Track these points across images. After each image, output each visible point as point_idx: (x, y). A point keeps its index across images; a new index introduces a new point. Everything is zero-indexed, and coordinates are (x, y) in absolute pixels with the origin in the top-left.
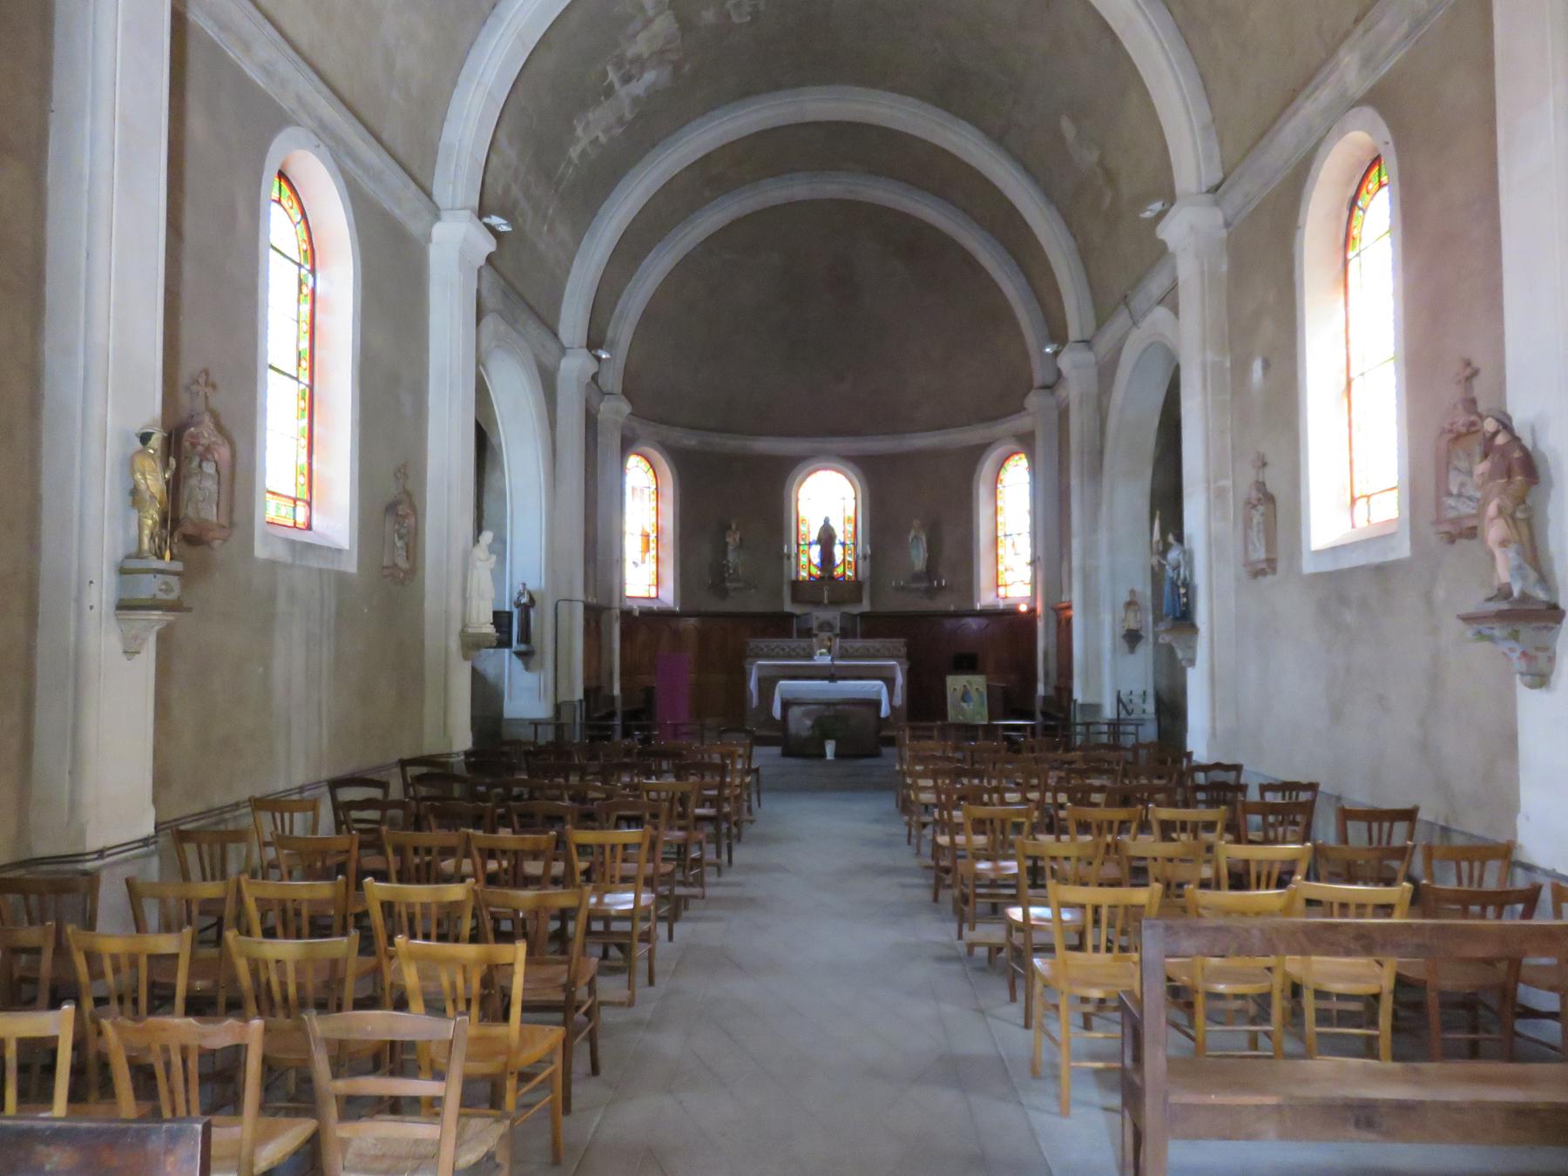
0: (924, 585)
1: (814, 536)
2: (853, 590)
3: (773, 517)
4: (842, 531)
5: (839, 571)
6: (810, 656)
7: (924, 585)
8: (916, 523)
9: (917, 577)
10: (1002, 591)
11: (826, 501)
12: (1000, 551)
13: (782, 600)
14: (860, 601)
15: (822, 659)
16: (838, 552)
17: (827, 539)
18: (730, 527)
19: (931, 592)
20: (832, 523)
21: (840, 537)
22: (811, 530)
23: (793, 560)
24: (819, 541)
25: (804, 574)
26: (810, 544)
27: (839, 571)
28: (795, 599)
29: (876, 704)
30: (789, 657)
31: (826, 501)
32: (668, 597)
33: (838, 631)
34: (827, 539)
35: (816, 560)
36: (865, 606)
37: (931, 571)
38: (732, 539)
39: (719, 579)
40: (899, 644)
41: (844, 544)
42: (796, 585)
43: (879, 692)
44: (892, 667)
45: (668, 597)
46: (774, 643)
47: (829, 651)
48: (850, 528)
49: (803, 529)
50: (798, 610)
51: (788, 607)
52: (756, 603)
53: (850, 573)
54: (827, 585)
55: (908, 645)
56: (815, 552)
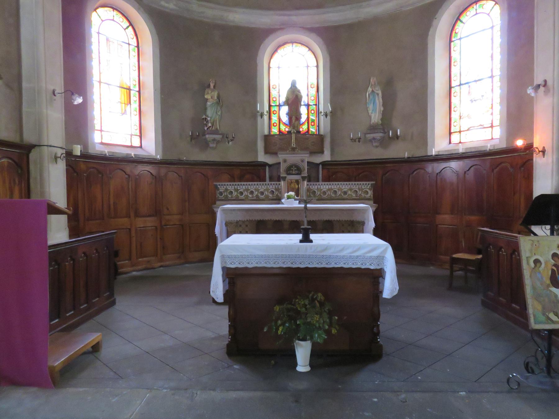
0: (378, 135)
1: (283, 99)
2: (316, 143)
3: (248, 81)
4: (307, 94)
5: (304, 128)
6: (278, 200)
7: (378, 135)
8: (373, 80)
9: (373, 128)
10: (455, 138)
11: (293, 70)
12: (455, 101)
13: (256, 152)
14: (322, 152)
15: (289, 203)
16: (303, 110)
17: (294, 100)
18: (209, 86)
19: (385, 142)
20: (299, 86)
21: (304, 100)
22: (280, 93)
23: (266, 118)
24: (287, 103)
25: (275, 130)
26: (279, 106)
27: (304, 128)
28: (267, 151)
29: (376, 276)
30: (258, 200)
31: (293, 70)
32: (151, 147)
33: (305, 174)
34: (294, 100)
35: (285, 119)
36: (327, 156)
37: (386, 123)
38: (211, 96)
39: (199, 135)
40: (366, 187)
41: (308, 105)
42: (268, 138)
43: (381, 258)
44: (363, 211)
45: (151, 147)
46: (243, 186)
47: (297, 194)
48: (313, 92)
49: (274, 93)
50: (269, 160)
51: (262, 157)
52: (234, 154)
53: (313, 130)
54: (295, 138)
55: (375, 189)
56: (285, 110)
